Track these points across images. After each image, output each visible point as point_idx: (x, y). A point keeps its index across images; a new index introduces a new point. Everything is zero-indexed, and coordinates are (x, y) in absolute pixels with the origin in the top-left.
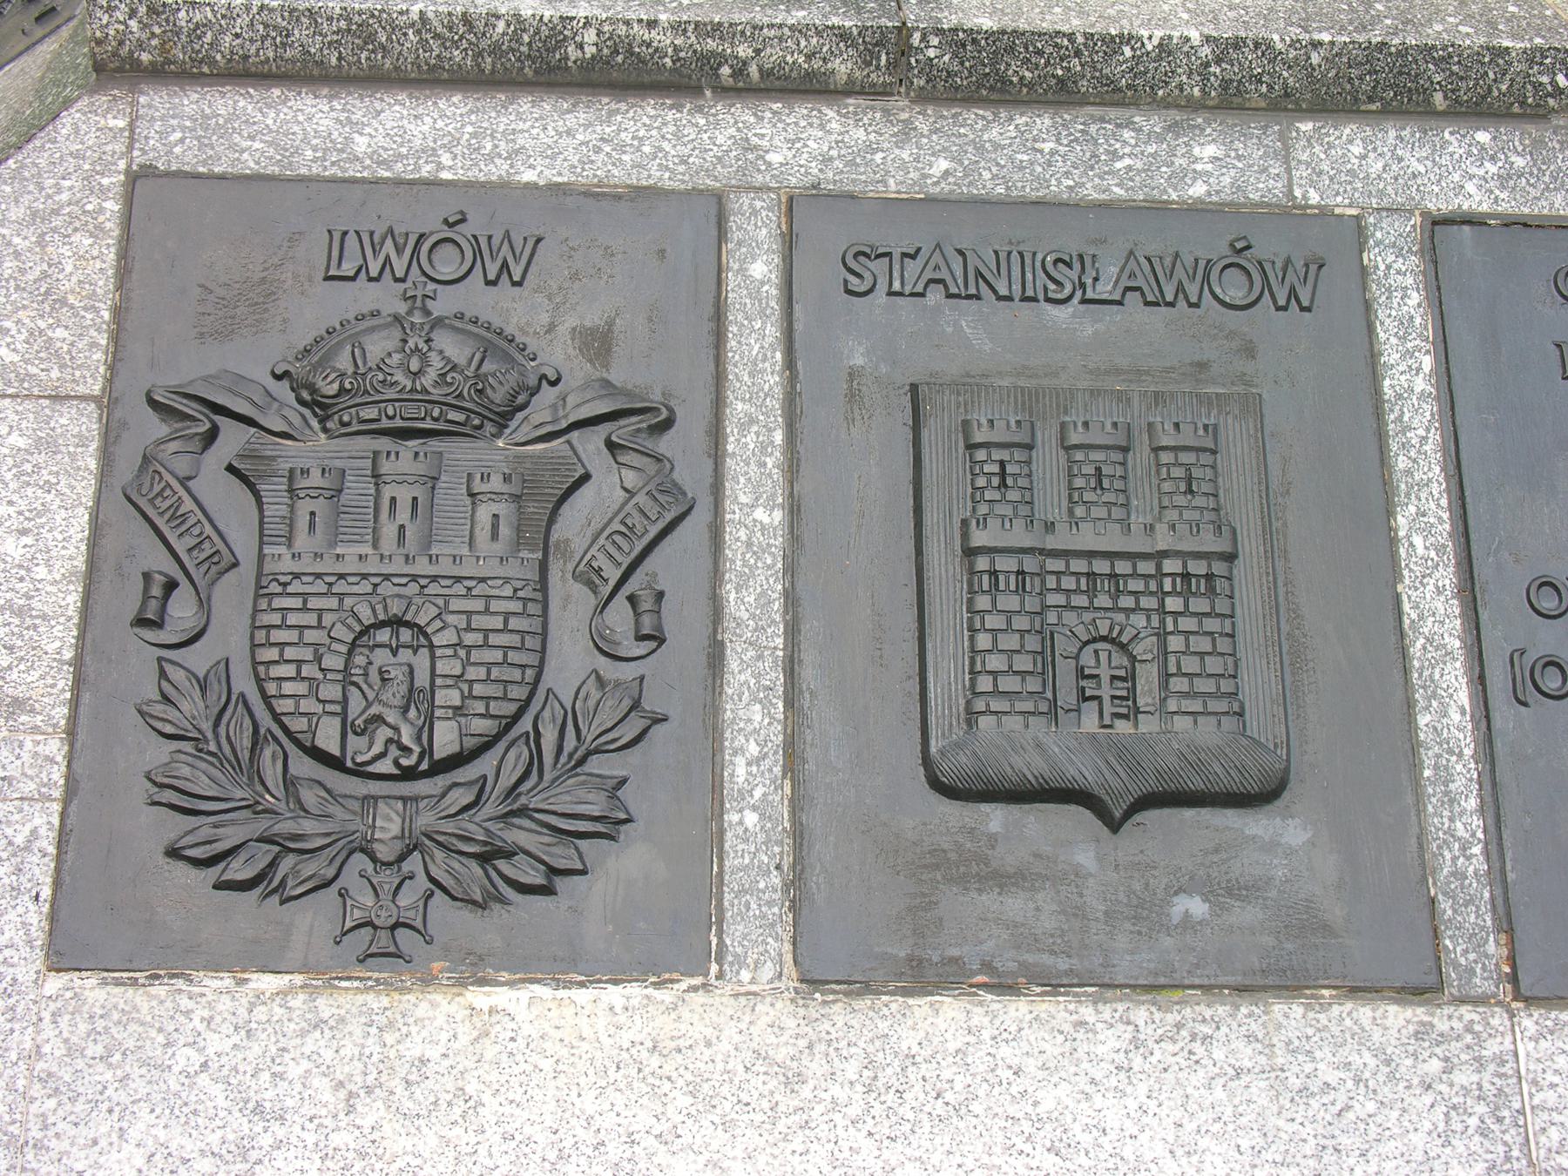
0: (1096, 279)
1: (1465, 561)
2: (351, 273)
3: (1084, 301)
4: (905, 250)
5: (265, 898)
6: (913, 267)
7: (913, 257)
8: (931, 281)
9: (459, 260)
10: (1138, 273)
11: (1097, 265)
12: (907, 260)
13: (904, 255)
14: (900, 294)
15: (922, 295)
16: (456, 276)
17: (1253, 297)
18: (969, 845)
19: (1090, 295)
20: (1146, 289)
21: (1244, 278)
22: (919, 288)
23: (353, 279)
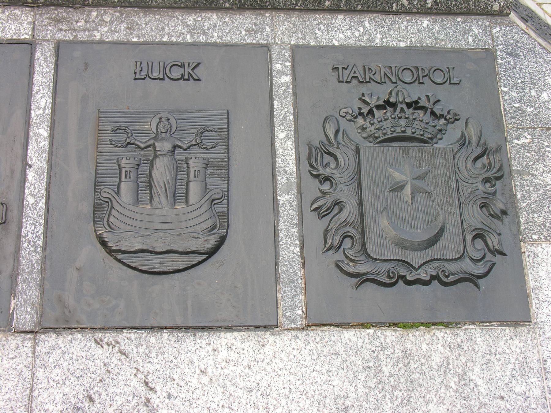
0: (141, 70)
1: (276, 246)
2: (143, 77)
3: (450, 84)
4: (344, 66)
5: (359, 286)
6: (346, 72)
7: (346, 69)
8: (353, 77)
9: (443, 78)
10: (357, 72)
11: (142, 66)
12: (344, 70)
13: (343, 68)
14: (342, 82)
15: (350, 82)
16: (177, 78)
17: (444, 81)
18: (51, 360)
19: (452, 82)
20: (359, 77)
21: (411, 74)
22: (349, 80)
23: (144, 79)
